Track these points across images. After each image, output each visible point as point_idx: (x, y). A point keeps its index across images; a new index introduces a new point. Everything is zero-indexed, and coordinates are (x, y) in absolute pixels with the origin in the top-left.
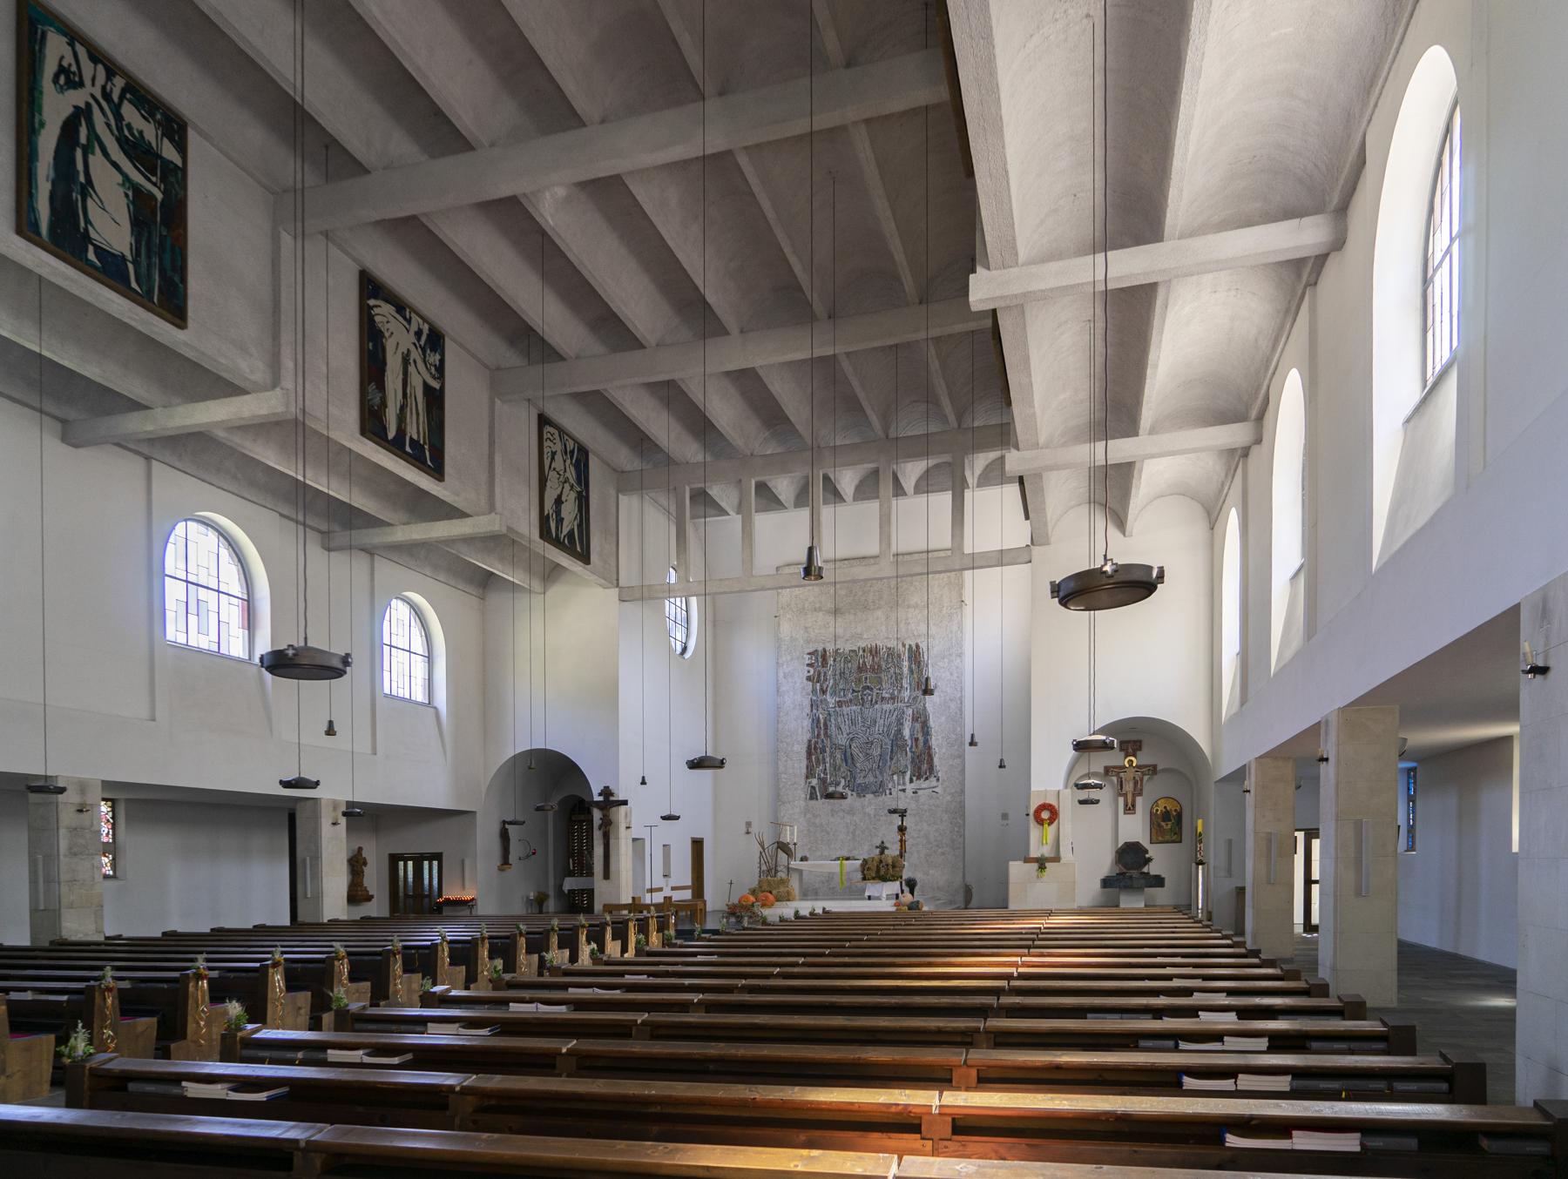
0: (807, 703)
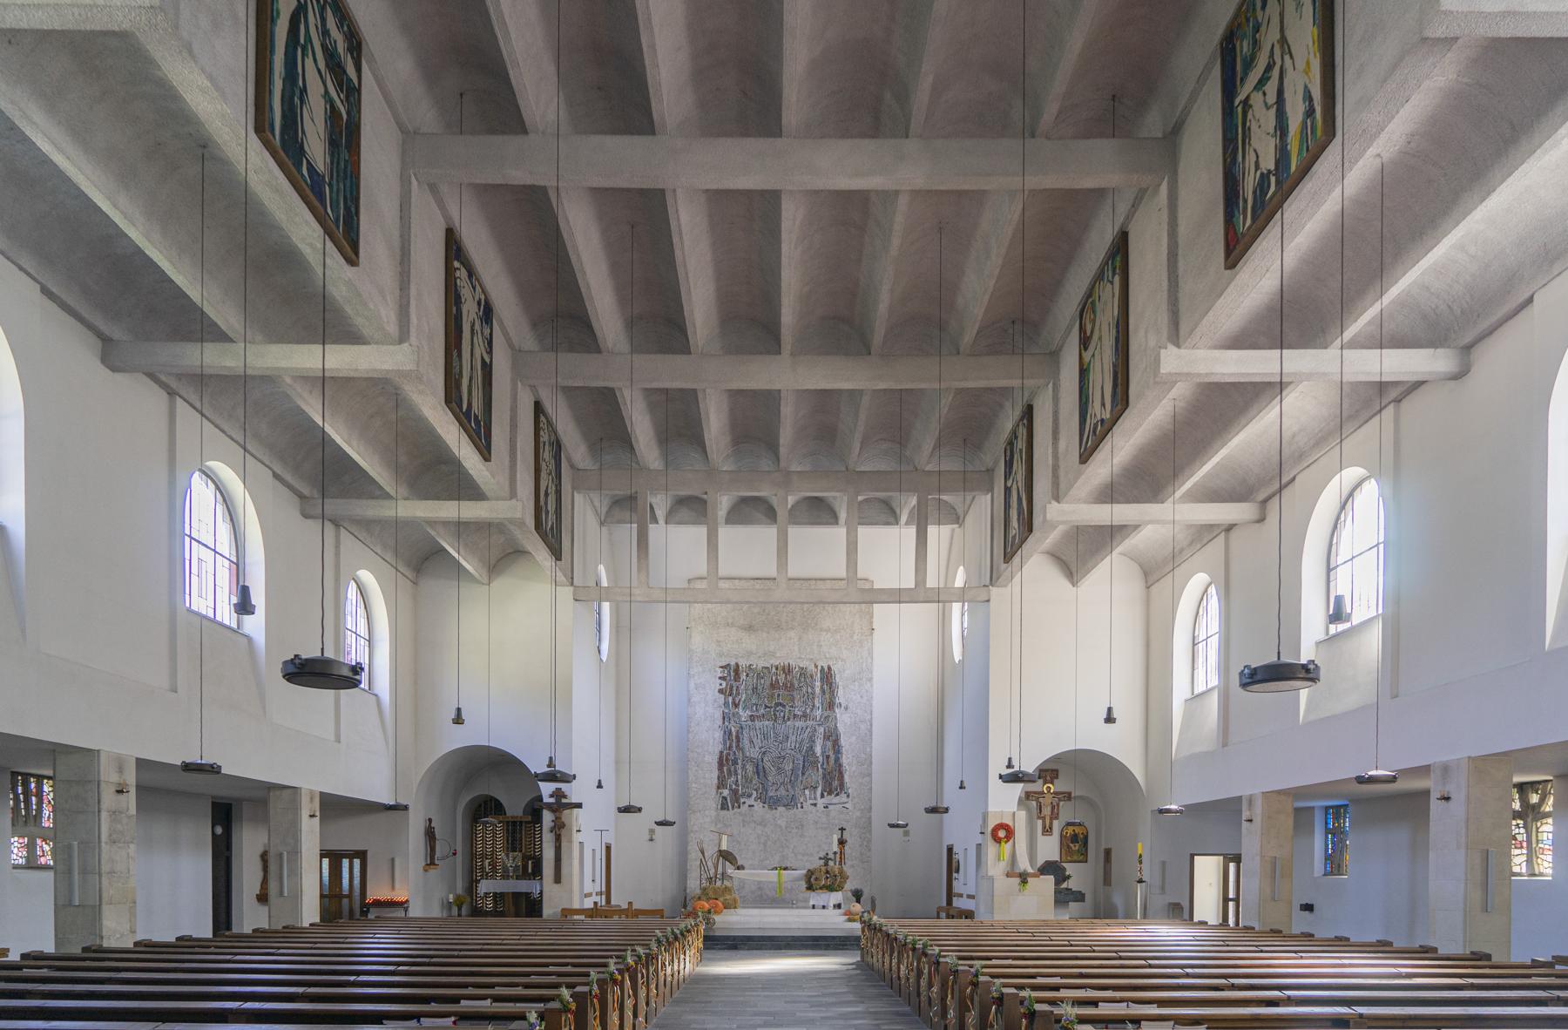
0: (718, 715)
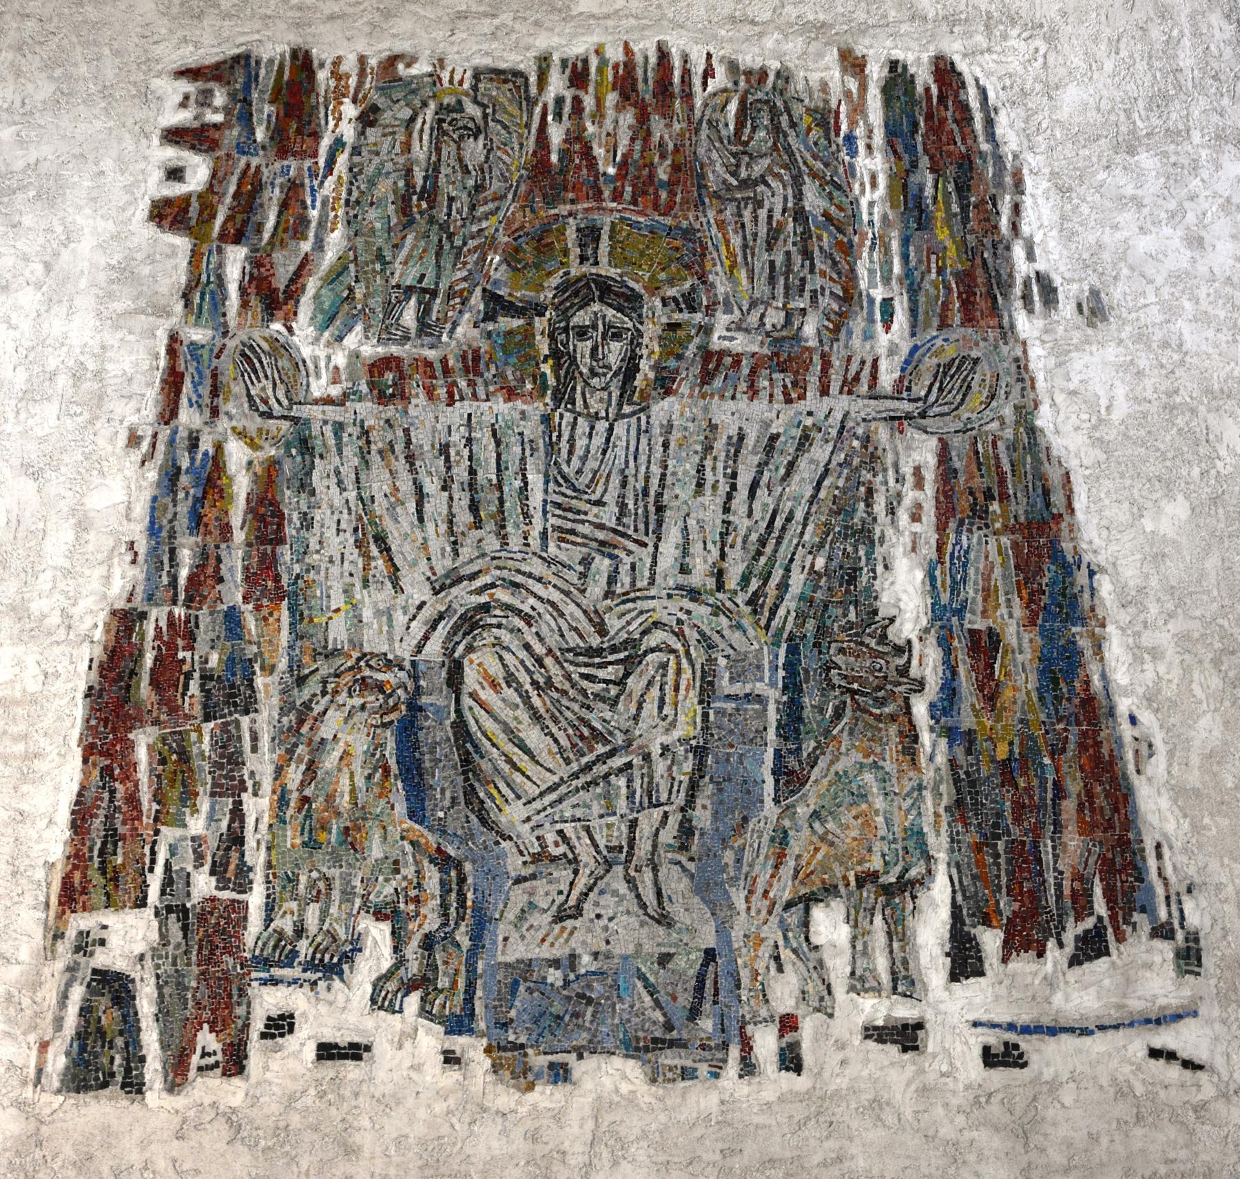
0: (136, 362)
